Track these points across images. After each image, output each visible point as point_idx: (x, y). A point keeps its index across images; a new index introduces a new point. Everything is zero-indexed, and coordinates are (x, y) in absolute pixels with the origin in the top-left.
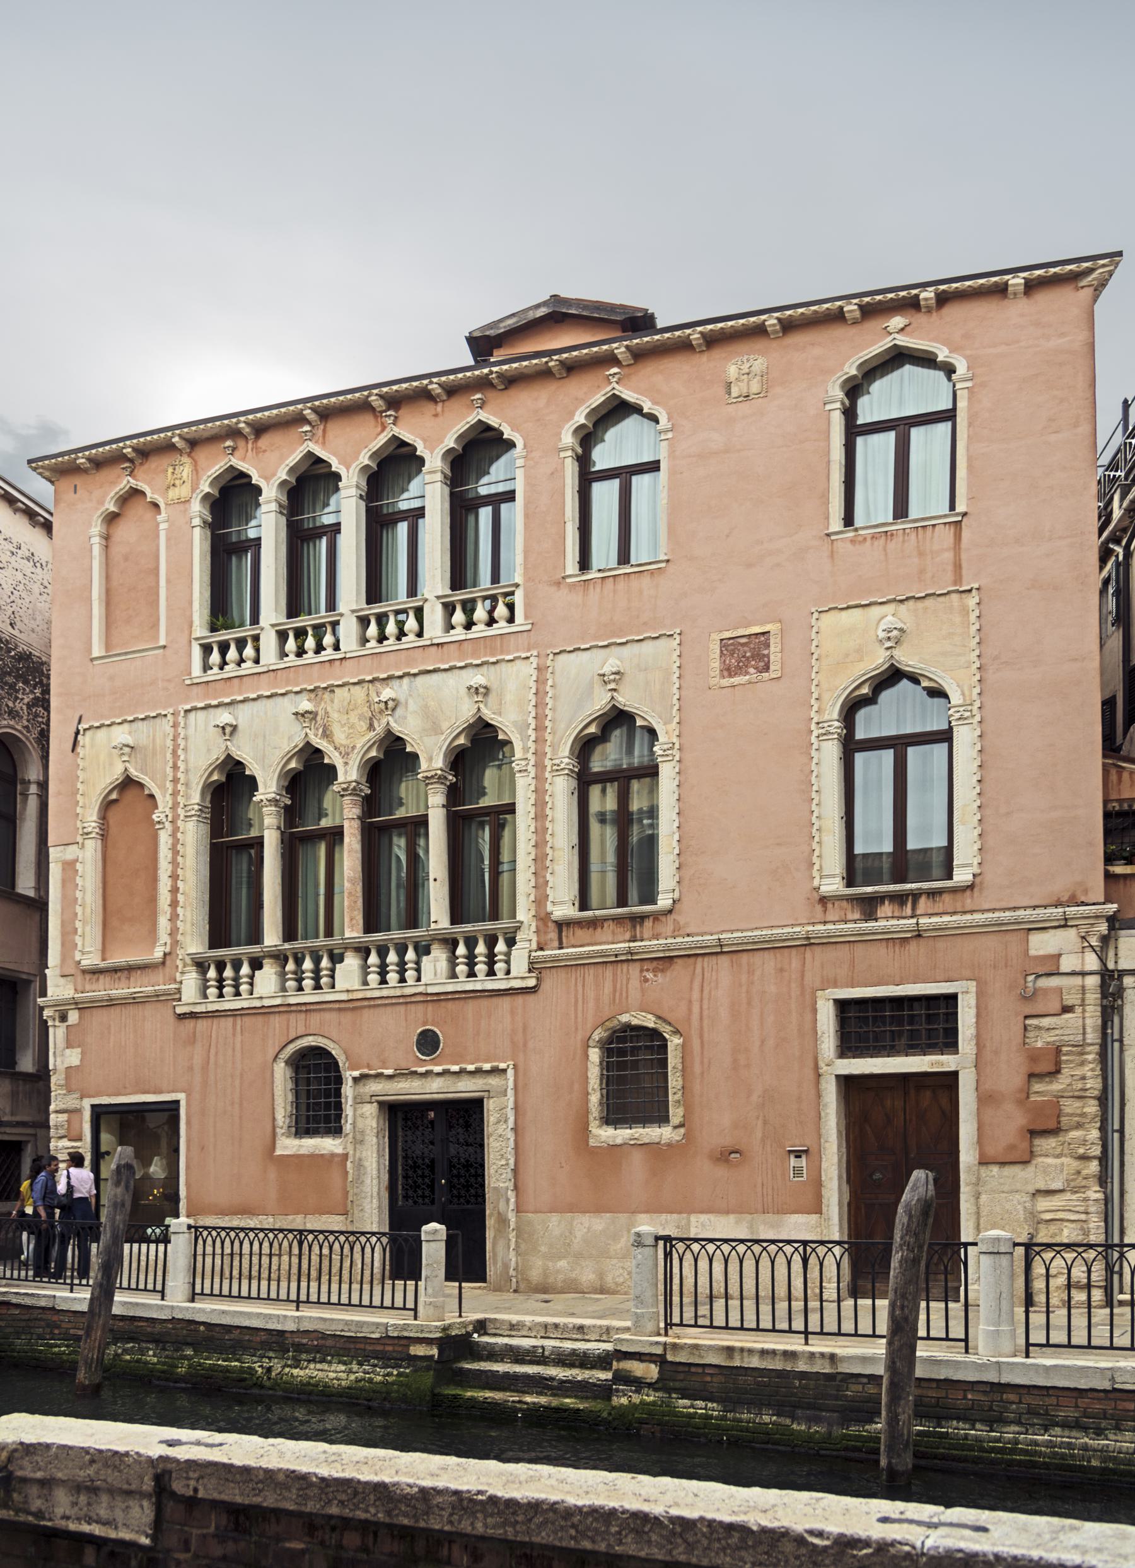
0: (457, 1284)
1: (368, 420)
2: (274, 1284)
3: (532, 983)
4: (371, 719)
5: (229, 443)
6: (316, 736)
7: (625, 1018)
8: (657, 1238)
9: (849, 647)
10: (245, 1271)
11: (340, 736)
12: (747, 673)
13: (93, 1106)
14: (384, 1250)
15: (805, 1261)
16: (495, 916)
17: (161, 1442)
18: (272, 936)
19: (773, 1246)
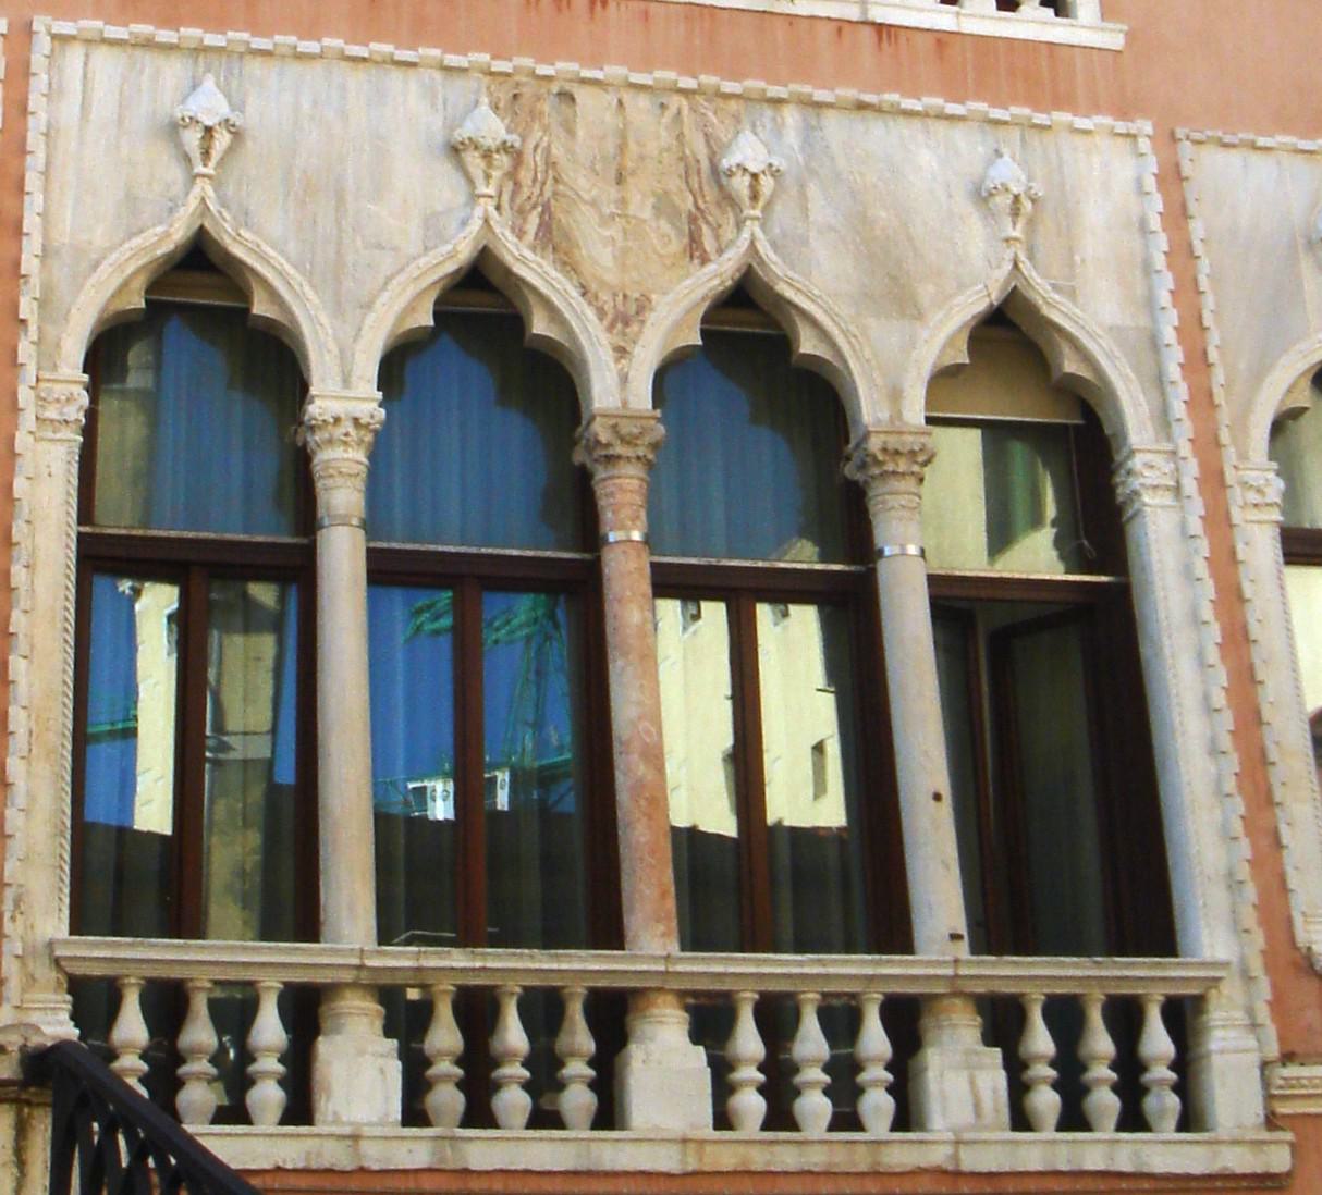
4: (692, 220)
6: (520, 233)
11: (598, 248)
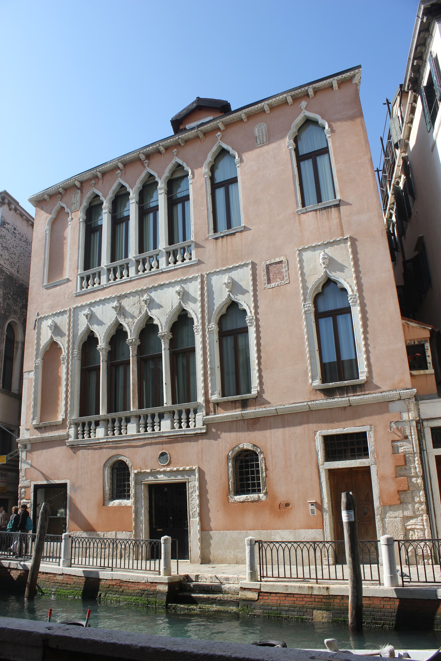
0: (176, 560)
1: (138, 165)
2: (103, 560)
3: (204, 431)
5: (93, 182)
7: (241, 446)
8: (256, 542)
9: (315, 268)
10: (91, 554)
12: (277, 281)
13: (34, 485)
14: (146, 547)
15: (315, 550)
16: (189, 401)
17: (46, 628)
18: (103, 411)
19: (369, 543)
